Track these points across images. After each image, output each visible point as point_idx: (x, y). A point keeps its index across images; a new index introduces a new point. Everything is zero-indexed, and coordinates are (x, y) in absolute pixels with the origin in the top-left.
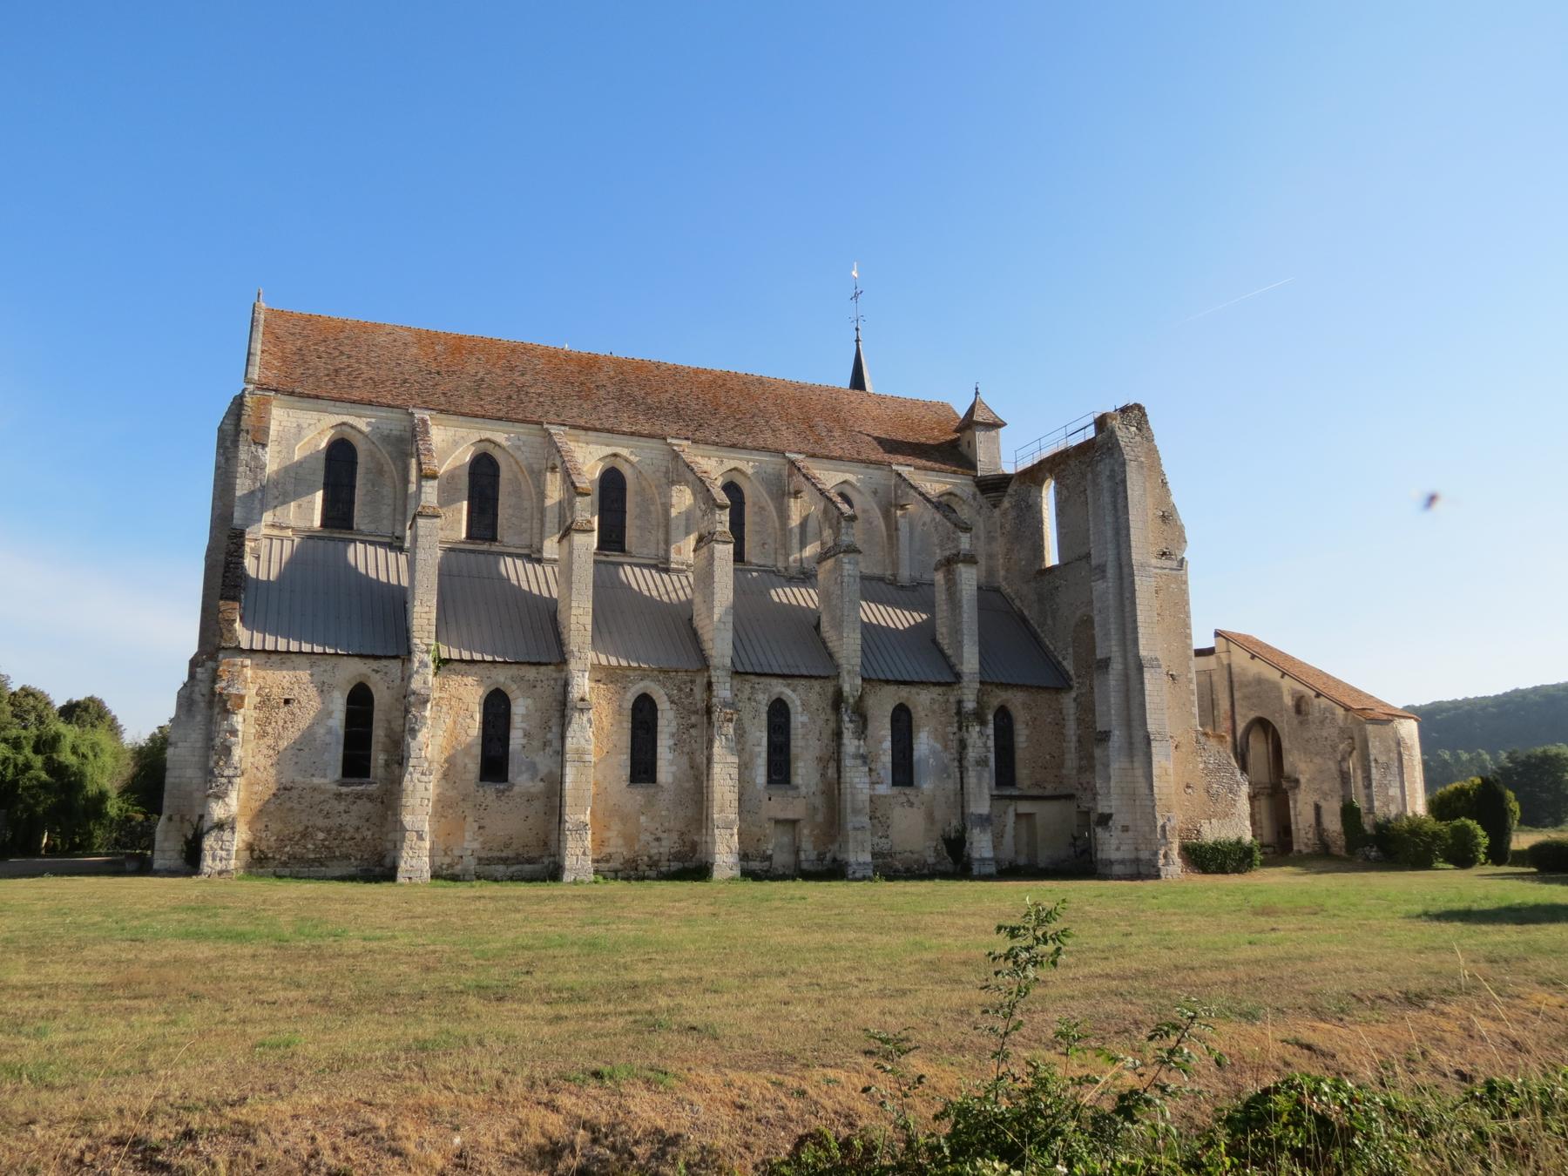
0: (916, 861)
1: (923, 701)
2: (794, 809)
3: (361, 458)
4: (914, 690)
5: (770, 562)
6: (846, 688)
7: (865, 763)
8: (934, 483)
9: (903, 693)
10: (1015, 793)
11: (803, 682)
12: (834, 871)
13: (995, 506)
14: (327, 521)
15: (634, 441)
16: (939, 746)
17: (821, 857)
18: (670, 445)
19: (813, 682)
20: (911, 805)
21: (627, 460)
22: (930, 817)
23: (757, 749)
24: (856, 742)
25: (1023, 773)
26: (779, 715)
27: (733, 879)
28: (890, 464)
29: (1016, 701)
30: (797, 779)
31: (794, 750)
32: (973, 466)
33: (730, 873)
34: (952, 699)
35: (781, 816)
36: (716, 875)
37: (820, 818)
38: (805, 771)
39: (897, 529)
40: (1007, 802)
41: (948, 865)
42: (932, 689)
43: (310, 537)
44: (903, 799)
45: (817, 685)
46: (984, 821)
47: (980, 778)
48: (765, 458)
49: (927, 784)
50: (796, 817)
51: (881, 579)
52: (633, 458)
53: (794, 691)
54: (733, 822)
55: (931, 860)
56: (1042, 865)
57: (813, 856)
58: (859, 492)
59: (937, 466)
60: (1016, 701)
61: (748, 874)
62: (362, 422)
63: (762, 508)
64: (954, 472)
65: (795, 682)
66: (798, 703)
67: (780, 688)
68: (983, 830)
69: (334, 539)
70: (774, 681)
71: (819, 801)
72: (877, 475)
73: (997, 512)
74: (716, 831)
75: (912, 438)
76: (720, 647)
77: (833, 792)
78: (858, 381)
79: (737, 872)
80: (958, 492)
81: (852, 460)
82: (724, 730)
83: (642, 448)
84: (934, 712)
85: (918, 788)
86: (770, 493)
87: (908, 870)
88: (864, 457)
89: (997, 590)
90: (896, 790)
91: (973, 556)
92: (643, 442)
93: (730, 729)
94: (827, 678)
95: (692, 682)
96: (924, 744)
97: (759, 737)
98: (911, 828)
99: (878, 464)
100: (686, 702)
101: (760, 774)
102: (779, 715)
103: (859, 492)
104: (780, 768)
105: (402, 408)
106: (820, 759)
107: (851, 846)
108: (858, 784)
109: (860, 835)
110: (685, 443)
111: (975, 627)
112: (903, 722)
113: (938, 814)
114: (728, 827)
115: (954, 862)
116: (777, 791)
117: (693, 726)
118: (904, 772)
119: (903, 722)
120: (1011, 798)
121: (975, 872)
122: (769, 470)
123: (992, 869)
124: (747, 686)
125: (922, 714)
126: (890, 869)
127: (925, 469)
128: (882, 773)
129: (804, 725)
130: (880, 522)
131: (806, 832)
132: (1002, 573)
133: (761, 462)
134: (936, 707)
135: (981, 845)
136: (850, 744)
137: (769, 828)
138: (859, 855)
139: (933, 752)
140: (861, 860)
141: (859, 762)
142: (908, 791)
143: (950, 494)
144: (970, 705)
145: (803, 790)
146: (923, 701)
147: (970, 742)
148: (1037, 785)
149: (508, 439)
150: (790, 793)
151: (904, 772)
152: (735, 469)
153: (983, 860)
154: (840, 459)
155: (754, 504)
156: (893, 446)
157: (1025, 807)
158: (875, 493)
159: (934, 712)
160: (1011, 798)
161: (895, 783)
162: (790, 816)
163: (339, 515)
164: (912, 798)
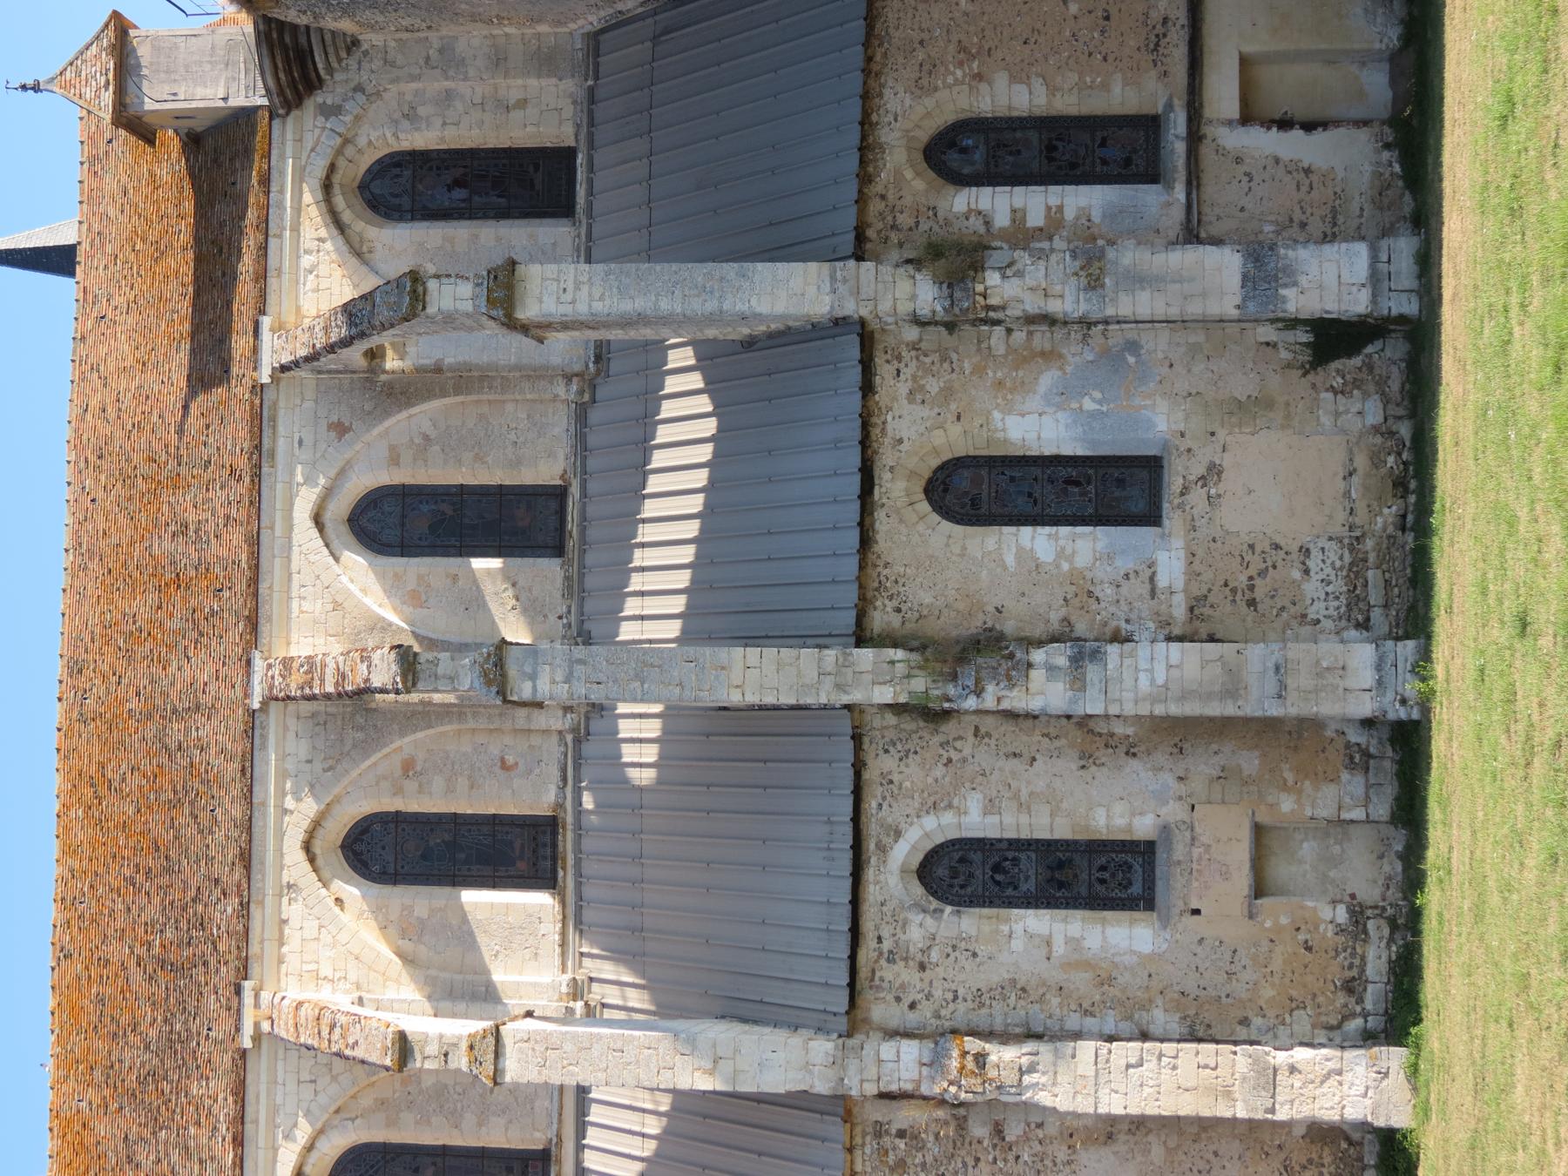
0: (1376, 460)
1: (917, 433)
2: (1224, 839)
3: (386, 477)
4: (886, 457)
5: (552, 751)
6: (884, 695)
7: (1096, 655)
8: (312, 275)
9: (898, 490)
10: (1178, 124)
11: (870, 805)
12: (1405, 745)
13: (355, 43)
14: (541, 875)
15: (257, 1133)
16: (1048, 379)
17: (1360, 760)
18: (264, 704)
19: (869, 775)
20: (1214, 471)
21: (310, 1148)
22: (1246, 411)
23: (1059, 948)
24: (1037, 675)
25: (1120, 96)
26: (970, 874)
27: (1413, 1071)
28: (258, 389)
29: (911, 113)
30: (1143, 827)
31: (1062, 830)
32: (245, 116)
33: (1398, 1078)
34: (912, 333)
35: (1242, 881)
36: (1400, 1118)
37: (1250, 762)
38: (1115, 805)
39: (438, 369)
40: (1206, 151)
41: (1388, 354)
42: (882, 396)
43: (576, 919)
44: (1197, 496)
45: (879, 764)
46: (1263, 273)
47: (1138, 280)
48: (270, 764)
49: (1155, 421)
50: (1245, 834)
51: (581, 415)
52: (304, 1132)
53: (898, 834)
54: (1258, 1064)
55: (1374, 413)
56: (1393, 35)
57: (1354, 784)
58: (342, 473)
59: (250, 243)
60: (911, 113)
61: (1398, 1018)
62: (291, 814)
63: (408, 766)
64: (265, 181)
65: (872, 830)
66: (930, 822)
67: (891, 876)
68: (1288, 275)
69: (578, 862)
70: (872, 893)
71: (1202, 765)
72: (293, 423)
73: (370, 39)
74: (1282, 1115)
75: (181, 264)
76: (784, 1061)
77: (1176, 734)
78: (57, 260)
79: (1395, 1057)
80: (319, 167)
81: (256, 502)
82: (1009, 1077)
83: (274, 1111)
84: (948, 393)
85: (1166, 445)
86: (365, 748)
87: (1400, 486)
88: (242, 463)
89: (594, 41)
90: (1172, 519)
91: (493, 274)
92: (258, 1108)
93: (1004, 1056)
94: (857, 738)
95: (879, 1131)
96: (1038, 425)
97: (1034, 937)
98: (1276, 481)
99: (259, 422)
100: (934, 1149)
101: (1123, 937)
102: (970, 874)
103: (342, 473)
104: (1107, 875)
105: (252, 723)
106: (1087, 759)
107: (1327, 708)
108: (1150, 675)
109: (1301, 680)
110: (259, 664)
111: (699, 272)
112: (983, 489)
113: (1242, 385)
114: (1269, 1078)
115: (1387, 354)
116: (1175, 886)
117: (998, 1131)
118: (1114, 489)
119: (983, 489)
120: (1194, 138)
121: (1408, 306)
122: (301, 749)
123: (1404, 247)
124: (887, 972)
125: (955, 430)
126: (1398, 591)
127: (262, 276)
128: (1124, 564)
129: (991, 807)
130: (423, 415)
131: (1287, 804)
132: (543, 28)
133: (283, 775)
134: (933, 386)
135: (1334, 279)
136: (1044, 689)
137: (1276, 912)
138: (1350, 679)
139: (1064, 395)
140: (1368, 678)
141: (1092, 672)
142: (1173, 483)
143: (327, 187)
144: (925, 294)
145: (1174, 812)
146: (917, 433)
147: (1033, 304)
148: (1156, 46)
149: (309, 481)
150: (1179, 851)
151: (1114, 489)
152: (307, 847)
153: (1376, 280)
154: (254, 542)
155: (398, 791)
156: (210, 359)
157: (1223, 95)
158: (340, 429)
159: (948, 393)
160: (1194, 138)
161: (1151, 517)
162: (1240, 854)
163: (514, 851)
164: (1199, 470)
